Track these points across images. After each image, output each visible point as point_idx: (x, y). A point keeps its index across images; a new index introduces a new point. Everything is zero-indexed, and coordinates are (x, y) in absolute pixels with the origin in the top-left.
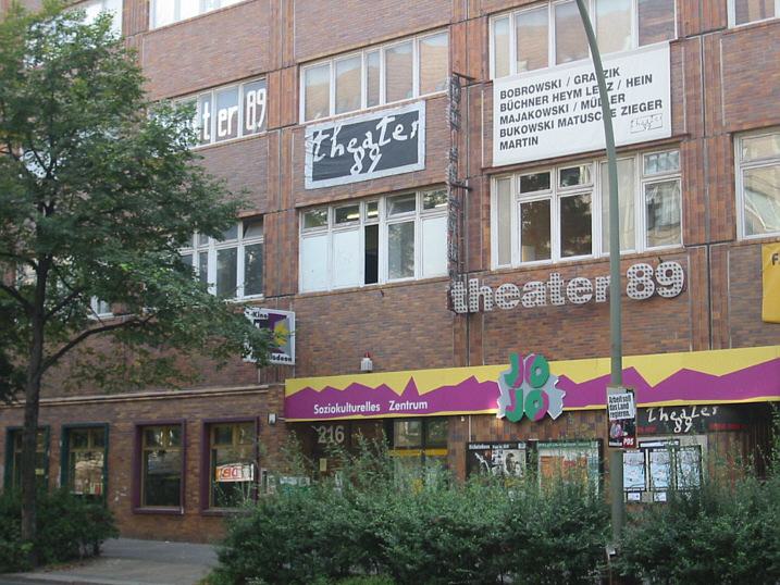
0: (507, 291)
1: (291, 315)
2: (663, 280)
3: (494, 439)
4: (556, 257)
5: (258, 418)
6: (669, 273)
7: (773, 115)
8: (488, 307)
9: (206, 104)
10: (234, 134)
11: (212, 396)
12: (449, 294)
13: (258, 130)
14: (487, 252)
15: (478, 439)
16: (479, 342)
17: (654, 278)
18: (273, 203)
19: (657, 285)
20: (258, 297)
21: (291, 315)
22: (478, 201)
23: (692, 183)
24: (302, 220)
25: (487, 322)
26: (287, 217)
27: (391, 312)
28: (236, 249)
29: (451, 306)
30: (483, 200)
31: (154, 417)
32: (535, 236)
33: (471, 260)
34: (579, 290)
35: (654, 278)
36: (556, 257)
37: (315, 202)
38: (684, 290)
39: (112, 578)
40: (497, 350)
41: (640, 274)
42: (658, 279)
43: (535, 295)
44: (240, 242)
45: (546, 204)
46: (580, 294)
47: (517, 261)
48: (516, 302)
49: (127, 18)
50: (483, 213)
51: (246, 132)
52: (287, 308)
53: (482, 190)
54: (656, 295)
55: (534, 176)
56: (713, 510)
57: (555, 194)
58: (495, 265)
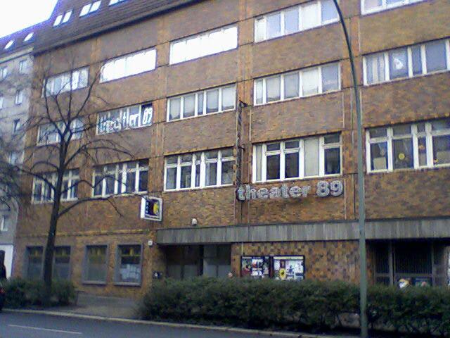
0: (296, 189)
1: (160, 200)
2: (333, 188)
3: (253, 254)
4: (219, 184)
5: (29, 249)
6: (336, 186)
7: (100, 160)
8: (254, 198)
9: (125, 113)
10: (137, 125)
11: (122, 234)
12: (236, 192)
13: (147, 124)
14: (251, 176)
15: (246, 254)
16: (247, 213)
17: (329, 187)
18: (154, 153)
19: (331, 190)
20: (145, 192)
21: (160, 200)
22: (248, 154)
23: (347, 148)
24: (166, 161)
25: (250, 204)
26: (159, 159)
27: (206, 200)
28: (387, 143)
29: (237, 197)
30: (250, 154)
31: (94, 243)
32: (273, 171)
33: (244, 179)
34: (296, 192)
35: (329, 187)
36: (178, 188)
37: (173, 153)
38: (343, 193)
39: (241, 333)
40: (255, 217)
41: (323, 186)
42: (331, 188)
43: (275, 193)
44: (137, 170)
45: (176, 169)
46: (296, 193)
47: (264, 180)
48: (267, 196)
49: (124, 80)
50: (250, 160)
51: (142, 124)
52: (158, 197)
53: (250, 149)
54: (330, 195)
55: (273, 144)
56: (310, 295)
57: (282, 152)
58: (254, 181)
